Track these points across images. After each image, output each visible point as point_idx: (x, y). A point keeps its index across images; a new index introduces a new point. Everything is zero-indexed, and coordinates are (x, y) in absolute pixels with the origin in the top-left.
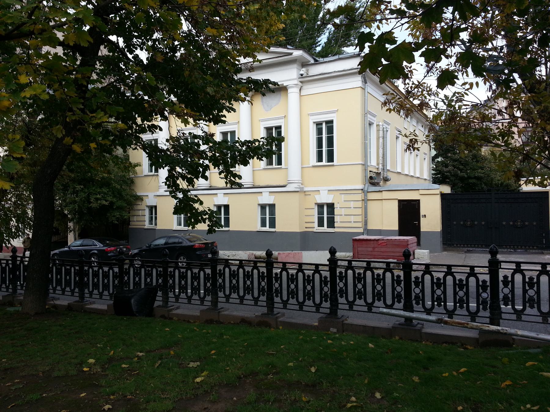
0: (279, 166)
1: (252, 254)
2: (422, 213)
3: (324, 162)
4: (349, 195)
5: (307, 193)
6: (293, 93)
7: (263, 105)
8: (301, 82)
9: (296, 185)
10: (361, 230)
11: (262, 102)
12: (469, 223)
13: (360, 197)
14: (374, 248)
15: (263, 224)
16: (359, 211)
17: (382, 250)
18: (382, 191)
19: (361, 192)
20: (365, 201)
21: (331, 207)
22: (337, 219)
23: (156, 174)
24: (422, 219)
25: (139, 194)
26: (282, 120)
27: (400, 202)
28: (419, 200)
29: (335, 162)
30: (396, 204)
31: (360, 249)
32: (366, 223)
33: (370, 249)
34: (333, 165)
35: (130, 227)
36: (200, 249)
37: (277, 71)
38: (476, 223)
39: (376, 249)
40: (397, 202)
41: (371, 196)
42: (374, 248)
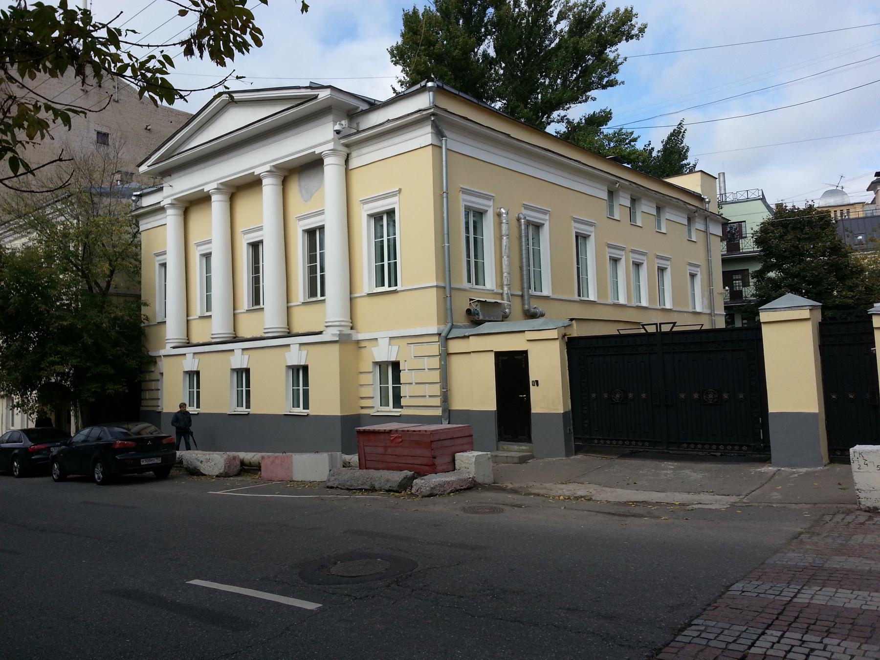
0: (258, 307)
1: (234, 458)
2: (532, 377)
3: (319, 298)
4: (425, 346)
5: (363, 344)
6: (332, 168)
7: (301, 191)
8: (347, 146)
9: (335, 331)
10: (438, 412)
11: (300, 186)
12: (618, 396)
13: (435, 349)
14: (386, 448)
15: (239, 404)
16: (436, 376)
17: (398, 451)
18: (468, 337)
19: (436, 339)
20: (446, 355)
21: (396, 365)
22: (405, 391)
23: (323, 298)
24: (532, 389)
25: (152, 353)
26: (396, 199)
27: (498, 355)
28: (526, 352)
29: (399, 288)
30: (491, 359)
31: (368, 450)
32: (446, 397)
33: (381, 450)
34: (395, 292)
35: (142, 408)
36: (124, 450)
37: (228, 159)
38: (696, 396)
39: (390, 451)
40: (492, 357)
41: (455, 346)
42: (386, 448)
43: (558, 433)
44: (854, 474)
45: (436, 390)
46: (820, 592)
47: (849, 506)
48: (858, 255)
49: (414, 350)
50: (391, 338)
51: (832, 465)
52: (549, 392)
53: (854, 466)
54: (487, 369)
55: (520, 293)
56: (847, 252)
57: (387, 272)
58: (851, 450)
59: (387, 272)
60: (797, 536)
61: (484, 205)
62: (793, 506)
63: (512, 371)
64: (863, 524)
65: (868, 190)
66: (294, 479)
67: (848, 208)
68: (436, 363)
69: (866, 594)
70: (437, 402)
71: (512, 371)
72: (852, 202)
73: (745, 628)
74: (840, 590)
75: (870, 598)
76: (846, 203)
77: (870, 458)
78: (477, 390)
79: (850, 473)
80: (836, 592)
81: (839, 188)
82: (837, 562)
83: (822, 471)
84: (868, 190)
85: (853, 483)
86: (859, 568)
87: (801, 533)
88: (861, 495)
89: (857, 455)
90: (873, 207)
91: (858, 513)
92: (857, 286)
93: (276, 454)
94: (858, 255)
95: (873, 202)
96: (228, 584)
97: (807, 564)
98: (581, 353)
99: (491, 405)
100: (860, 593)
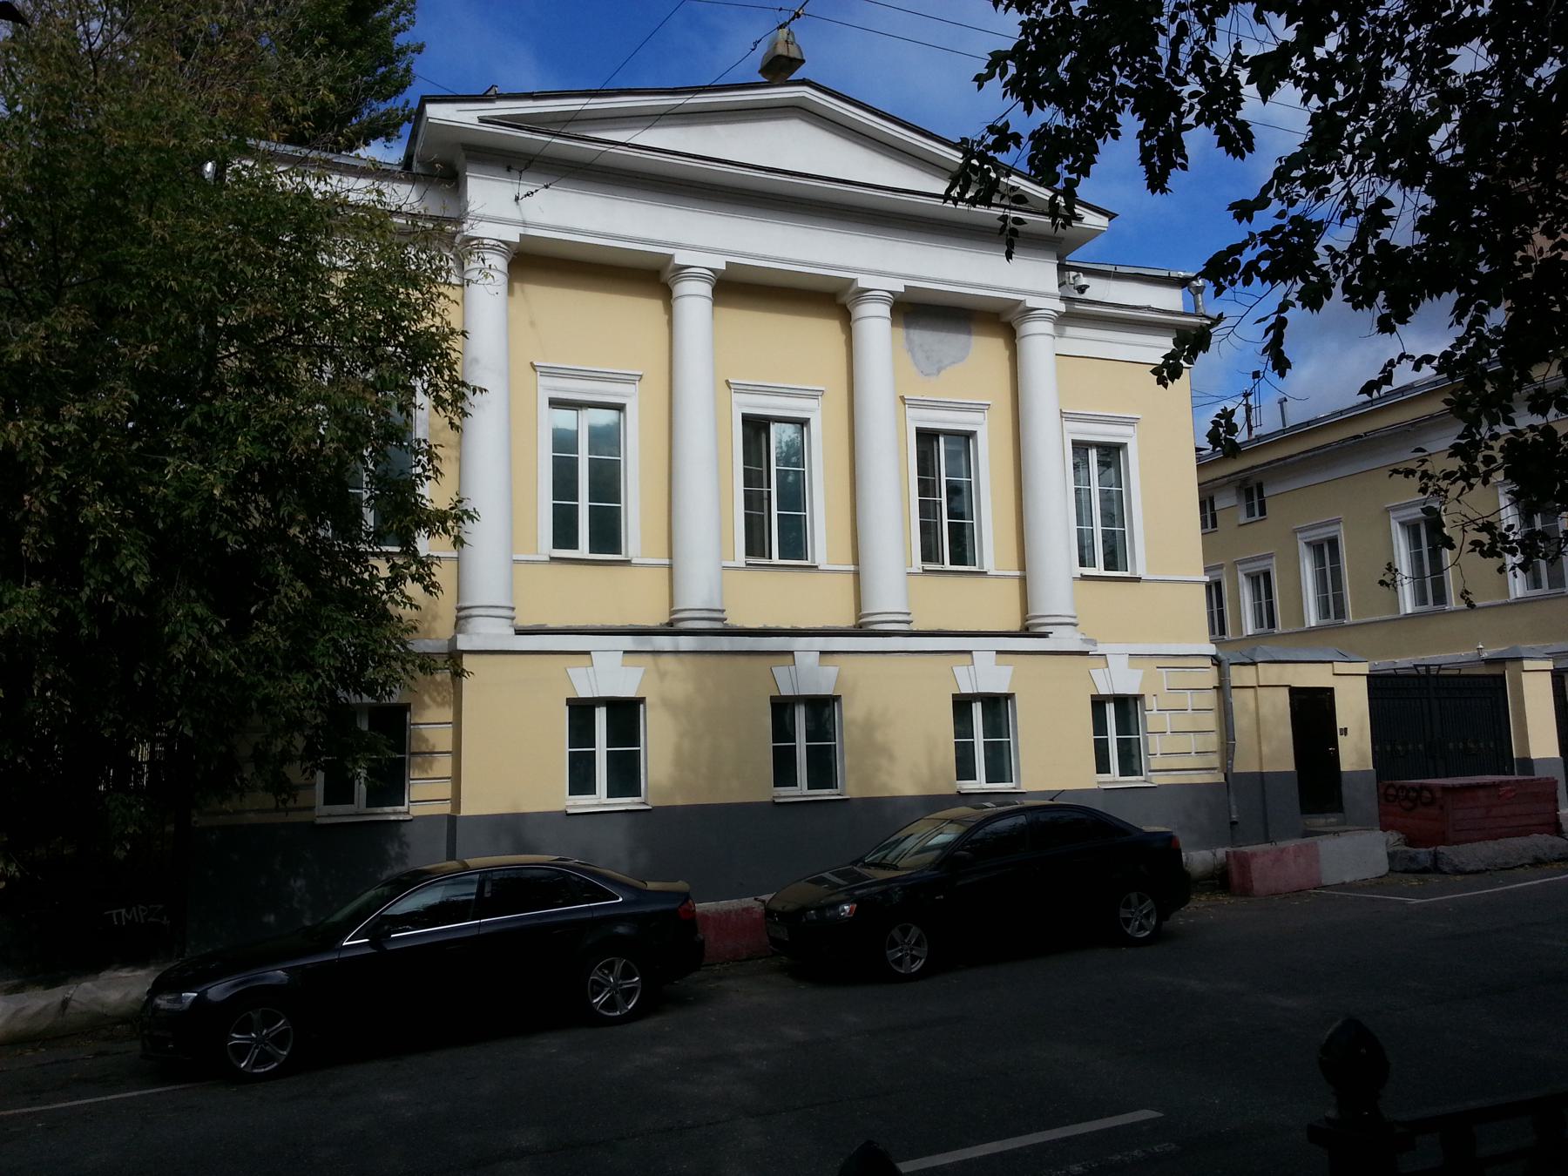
2: (1340, 725)
13: (1210, 677)
20: (1223, 688)
24: (1340, 738)
43: (1372, 806)
45: (1213, 742)
49: (1165, 679)
50: (998, 652)
52: (1355, 747)
54: (1278, 707)
55: (667, 561)
57: (1109, 550)
59: (1109, 550)
61: (615, 395)
63: (1313, 709)
66: (1324, 882)
68: (1210, 699)
70: (1215, 761)
71: (1313, 709)
78: (1271, 746)
93: (1282, 844)
98: (1381, 687)
99: (1289, 765)
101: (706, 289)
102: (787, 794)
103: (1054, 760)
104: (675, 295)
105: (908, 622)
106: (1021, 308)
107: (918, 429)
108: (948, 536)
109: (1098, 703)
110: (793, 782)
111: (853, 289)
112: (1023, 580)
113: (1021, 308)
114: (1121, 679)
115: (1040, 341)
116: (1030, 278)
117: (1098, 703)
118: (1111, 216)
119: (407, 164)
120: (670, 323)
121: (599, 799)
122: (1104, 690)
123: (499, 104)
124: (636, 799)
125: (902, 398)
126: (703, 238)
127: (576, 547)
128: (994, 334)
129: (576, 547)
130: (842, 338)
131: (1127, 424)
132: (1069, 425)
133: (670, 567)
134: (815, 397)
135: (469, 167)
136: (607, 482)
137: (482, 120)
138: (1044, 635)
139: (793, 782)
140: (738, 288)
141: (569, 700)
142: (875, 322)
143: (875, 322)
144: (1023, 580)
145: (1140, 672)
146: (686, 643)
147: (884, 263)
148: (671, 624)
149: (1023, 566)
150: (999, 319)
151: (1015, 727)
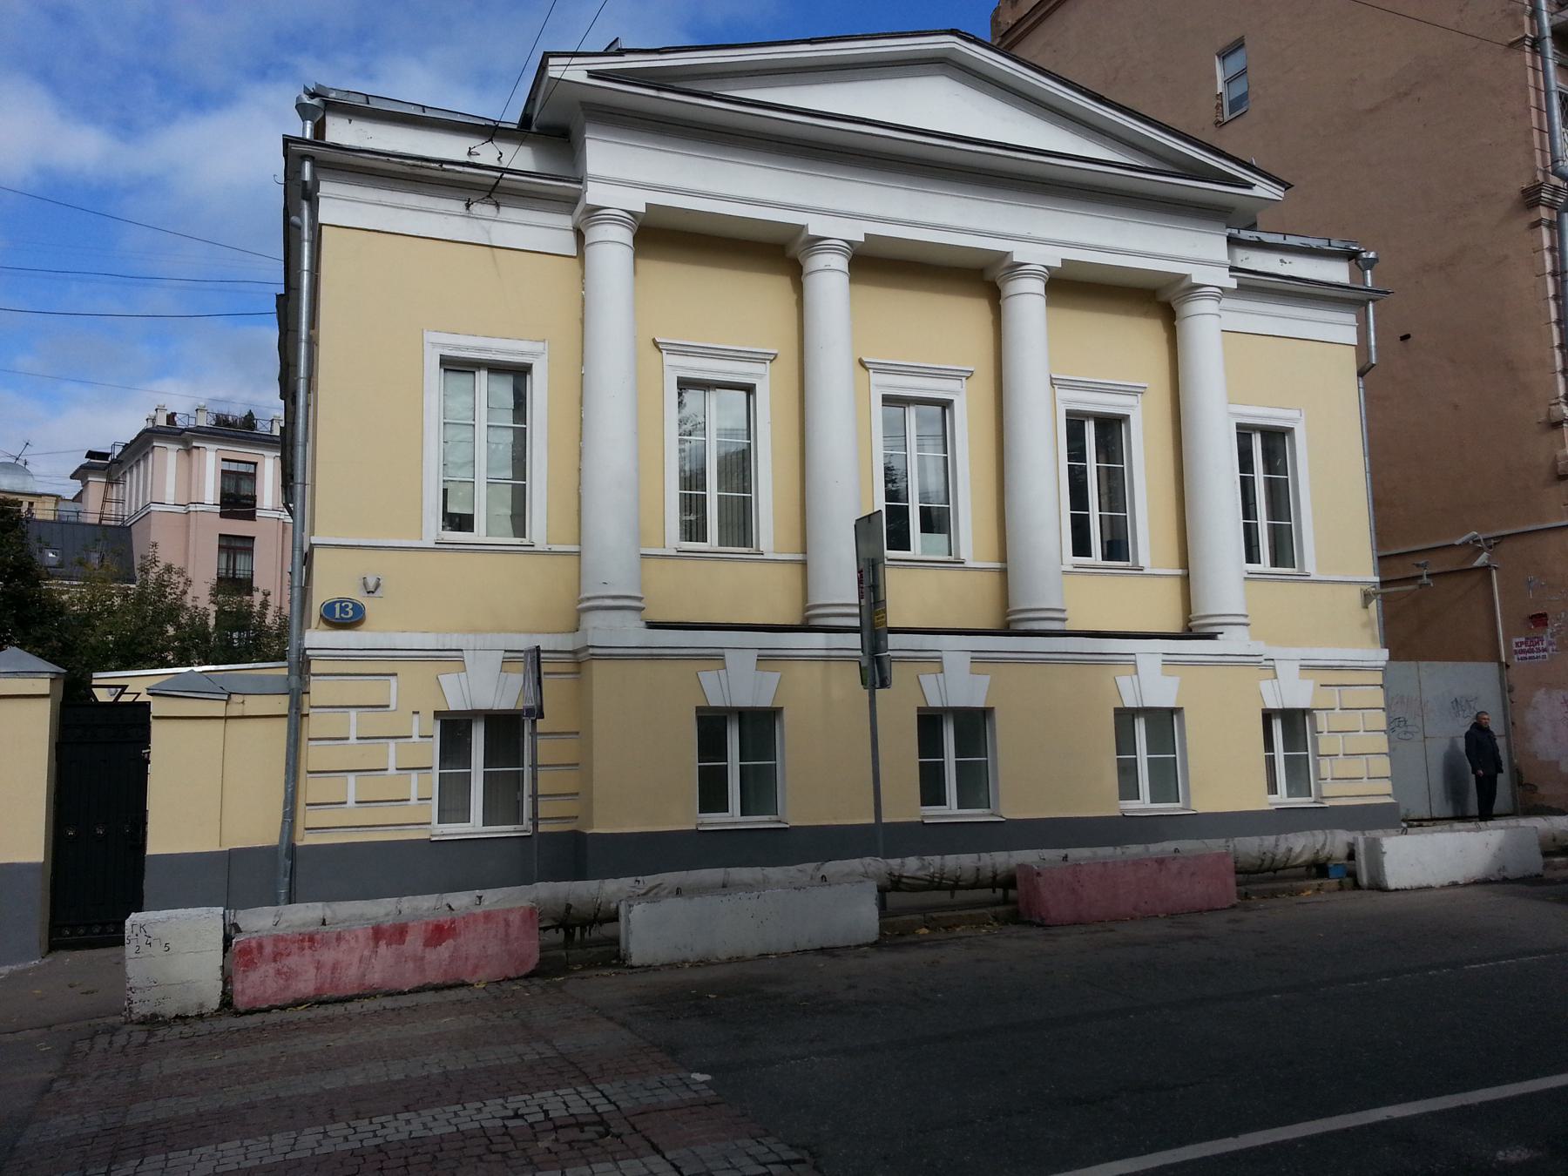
44: (129, 962)
46: (144, 1167)
47: (110, 1020)
48: (53, 584)
51: (55, 955)
53: (130, 949)
56: (39, 578)
58: (128, 923)
60: (47, 1088)
62: (9, 1038)
64: (145, 1044)
65: (72, 477)
67: (31, 499)
69: (210, 1149)
72: (39, 491)
73: (794, 1155)
74: (171, 1155)
75: (219, 1155)
76: (29, 489)
77: (155, 931)
79: (121, 963)
80: (167, 1159)
81: (21, 463)
82: (141, 1114)
83: (38, 967)
84: (72, 477)
85: (124, 978)
86: (181, 1113)
87: (53, 1081)
88: (135, 998)
89: (136, 929)
90: (72, 507)
91: (128, 1028)
92: (49, 639)
94: (53, 584)
95: (78, 498)
96: (1201, 1140)
97: (95, 1129)
100: (202, 1150)
101: (625, 235)
102: (933, 813)
103: (1226, 775)
104: (806, 270)
105: (1064, 620)
106: (1185, 284)
107: (1069, 413)
108: (1102, 534)
109: (1268, 716)
110: (723, 807)
111: (803, 237)
112: (1186, 579)
113: (1185, 284)
114: (1294, 692)
115: (1207, 324)
116: (1194, 252)
117: (1268, 716)
118: (1287, 186)
119: (526, 120)
120: (583, 277)
121: (474, 826)
122: (1272, 704)
123: (628, 57)
124: (519, 827)
125: (862, 363)
126: (840, 209)
127: (705, 540)
128: (782, 272)
129: (705, 540)
130: (793, 298)
131: (1128, 393)
132: (1062, 394)
133: (804, 563)
134: (1135, 394)
135: (587, 125)
136: (738, 467)
137: (593, 74)
138: (1212, 636)
139: (723, 807)
140: (876, 263)
141: (698, 709)
142: (829, 278)
143: (829, 278)
144: (1186, 579)
145: (986, 679)
146: (817, 640)
147: (1040, 236)
148: (1008, 624)
149: (1185, 562)
150: (1158, 300)
151: (783, 750)
